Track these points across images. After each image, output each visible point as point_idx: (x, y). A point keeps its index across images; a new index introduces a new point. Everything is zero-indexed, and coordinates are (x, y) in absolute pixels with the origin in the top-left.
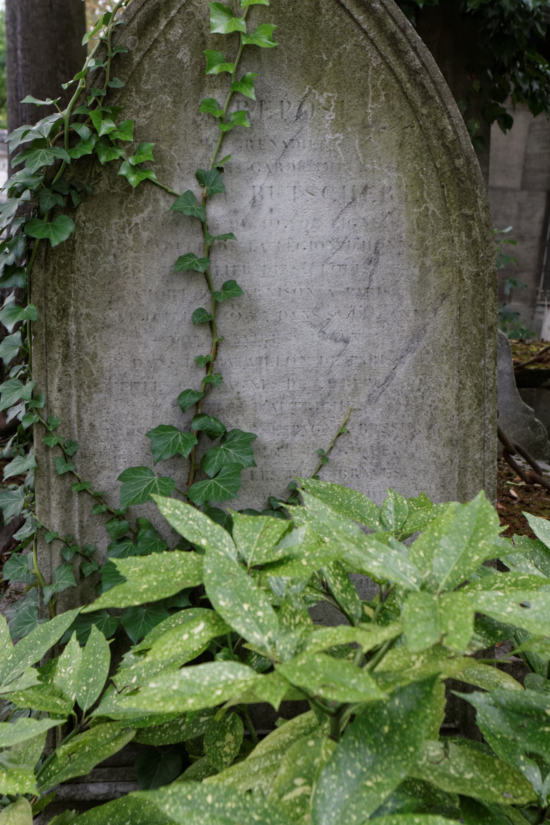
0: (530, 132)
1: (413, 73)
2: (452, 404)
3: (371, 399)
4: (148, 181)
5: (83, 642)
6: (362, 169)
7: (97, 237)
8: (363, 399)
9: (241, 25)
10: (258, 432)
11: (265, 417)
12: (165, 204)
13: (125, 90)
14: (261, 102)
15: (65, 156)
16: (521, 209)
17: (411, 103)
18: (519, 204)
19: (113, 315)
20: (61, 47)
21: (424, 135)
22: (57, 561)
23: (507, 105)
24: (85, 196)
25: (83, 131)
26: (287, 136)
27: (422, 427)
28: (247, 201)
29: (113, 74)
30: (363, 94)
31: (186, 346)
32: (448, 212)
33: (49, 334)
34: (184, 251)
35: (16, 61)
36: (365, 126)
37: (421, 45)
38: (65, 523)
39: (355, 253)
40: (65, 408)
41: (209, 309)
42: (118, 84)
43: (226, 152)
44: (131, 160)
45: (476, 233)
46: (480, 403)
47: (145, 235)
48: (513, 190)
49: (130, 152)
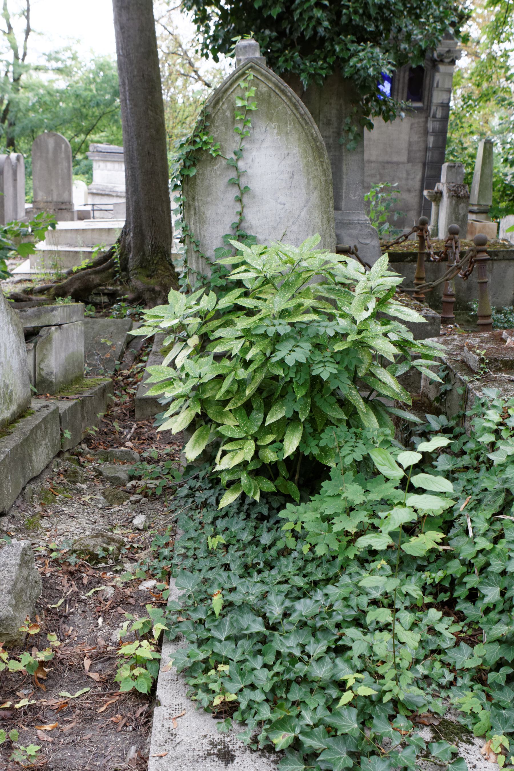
0: (411, 128)
1: (302, 115)
2: (320, 224)
3: (293, 223)
4: (218, 155)
5: (207, 295)
6: (287, 147)
7: (203, 174)
8: (291, 223)
9: (246, 103)
10: (257, 235)
11: (259, 230)
12: (224, 162)
13: (210, 126)
14: (253, 127)
15: (193, 148)
16: (408, 174)
17: (302, 125)
18: (407, 171)
19: (209, 199)
20: (149, 97)
21: (307, 135)
22: (195, 279)
23: (370, 118)
24: (199, 161)
25: (198, 140)
26: (262, 138)
27: (310, 231)
28: (250, 160)
29: (206, 121)
30: (286, 123)
31: (233, 208)
32: (315, 160)
33: (189, 206)
34: (231, 177)
35: (126, 106)
36: (287, 133)
37: (304, 106)
38: (197, 267)
39: (286, 175)
40: (196, 230)
41: (240, 195)
42: (208, 124)
43: (243, 144)
44: (213, 149)
45: (325, 167)
46: (329, 222)
47: (218, 173)
48: (403, 163)
49: (212, 146)
